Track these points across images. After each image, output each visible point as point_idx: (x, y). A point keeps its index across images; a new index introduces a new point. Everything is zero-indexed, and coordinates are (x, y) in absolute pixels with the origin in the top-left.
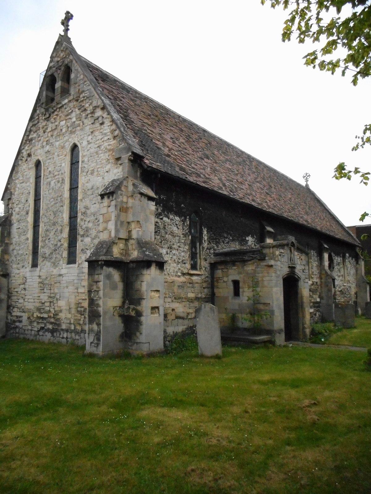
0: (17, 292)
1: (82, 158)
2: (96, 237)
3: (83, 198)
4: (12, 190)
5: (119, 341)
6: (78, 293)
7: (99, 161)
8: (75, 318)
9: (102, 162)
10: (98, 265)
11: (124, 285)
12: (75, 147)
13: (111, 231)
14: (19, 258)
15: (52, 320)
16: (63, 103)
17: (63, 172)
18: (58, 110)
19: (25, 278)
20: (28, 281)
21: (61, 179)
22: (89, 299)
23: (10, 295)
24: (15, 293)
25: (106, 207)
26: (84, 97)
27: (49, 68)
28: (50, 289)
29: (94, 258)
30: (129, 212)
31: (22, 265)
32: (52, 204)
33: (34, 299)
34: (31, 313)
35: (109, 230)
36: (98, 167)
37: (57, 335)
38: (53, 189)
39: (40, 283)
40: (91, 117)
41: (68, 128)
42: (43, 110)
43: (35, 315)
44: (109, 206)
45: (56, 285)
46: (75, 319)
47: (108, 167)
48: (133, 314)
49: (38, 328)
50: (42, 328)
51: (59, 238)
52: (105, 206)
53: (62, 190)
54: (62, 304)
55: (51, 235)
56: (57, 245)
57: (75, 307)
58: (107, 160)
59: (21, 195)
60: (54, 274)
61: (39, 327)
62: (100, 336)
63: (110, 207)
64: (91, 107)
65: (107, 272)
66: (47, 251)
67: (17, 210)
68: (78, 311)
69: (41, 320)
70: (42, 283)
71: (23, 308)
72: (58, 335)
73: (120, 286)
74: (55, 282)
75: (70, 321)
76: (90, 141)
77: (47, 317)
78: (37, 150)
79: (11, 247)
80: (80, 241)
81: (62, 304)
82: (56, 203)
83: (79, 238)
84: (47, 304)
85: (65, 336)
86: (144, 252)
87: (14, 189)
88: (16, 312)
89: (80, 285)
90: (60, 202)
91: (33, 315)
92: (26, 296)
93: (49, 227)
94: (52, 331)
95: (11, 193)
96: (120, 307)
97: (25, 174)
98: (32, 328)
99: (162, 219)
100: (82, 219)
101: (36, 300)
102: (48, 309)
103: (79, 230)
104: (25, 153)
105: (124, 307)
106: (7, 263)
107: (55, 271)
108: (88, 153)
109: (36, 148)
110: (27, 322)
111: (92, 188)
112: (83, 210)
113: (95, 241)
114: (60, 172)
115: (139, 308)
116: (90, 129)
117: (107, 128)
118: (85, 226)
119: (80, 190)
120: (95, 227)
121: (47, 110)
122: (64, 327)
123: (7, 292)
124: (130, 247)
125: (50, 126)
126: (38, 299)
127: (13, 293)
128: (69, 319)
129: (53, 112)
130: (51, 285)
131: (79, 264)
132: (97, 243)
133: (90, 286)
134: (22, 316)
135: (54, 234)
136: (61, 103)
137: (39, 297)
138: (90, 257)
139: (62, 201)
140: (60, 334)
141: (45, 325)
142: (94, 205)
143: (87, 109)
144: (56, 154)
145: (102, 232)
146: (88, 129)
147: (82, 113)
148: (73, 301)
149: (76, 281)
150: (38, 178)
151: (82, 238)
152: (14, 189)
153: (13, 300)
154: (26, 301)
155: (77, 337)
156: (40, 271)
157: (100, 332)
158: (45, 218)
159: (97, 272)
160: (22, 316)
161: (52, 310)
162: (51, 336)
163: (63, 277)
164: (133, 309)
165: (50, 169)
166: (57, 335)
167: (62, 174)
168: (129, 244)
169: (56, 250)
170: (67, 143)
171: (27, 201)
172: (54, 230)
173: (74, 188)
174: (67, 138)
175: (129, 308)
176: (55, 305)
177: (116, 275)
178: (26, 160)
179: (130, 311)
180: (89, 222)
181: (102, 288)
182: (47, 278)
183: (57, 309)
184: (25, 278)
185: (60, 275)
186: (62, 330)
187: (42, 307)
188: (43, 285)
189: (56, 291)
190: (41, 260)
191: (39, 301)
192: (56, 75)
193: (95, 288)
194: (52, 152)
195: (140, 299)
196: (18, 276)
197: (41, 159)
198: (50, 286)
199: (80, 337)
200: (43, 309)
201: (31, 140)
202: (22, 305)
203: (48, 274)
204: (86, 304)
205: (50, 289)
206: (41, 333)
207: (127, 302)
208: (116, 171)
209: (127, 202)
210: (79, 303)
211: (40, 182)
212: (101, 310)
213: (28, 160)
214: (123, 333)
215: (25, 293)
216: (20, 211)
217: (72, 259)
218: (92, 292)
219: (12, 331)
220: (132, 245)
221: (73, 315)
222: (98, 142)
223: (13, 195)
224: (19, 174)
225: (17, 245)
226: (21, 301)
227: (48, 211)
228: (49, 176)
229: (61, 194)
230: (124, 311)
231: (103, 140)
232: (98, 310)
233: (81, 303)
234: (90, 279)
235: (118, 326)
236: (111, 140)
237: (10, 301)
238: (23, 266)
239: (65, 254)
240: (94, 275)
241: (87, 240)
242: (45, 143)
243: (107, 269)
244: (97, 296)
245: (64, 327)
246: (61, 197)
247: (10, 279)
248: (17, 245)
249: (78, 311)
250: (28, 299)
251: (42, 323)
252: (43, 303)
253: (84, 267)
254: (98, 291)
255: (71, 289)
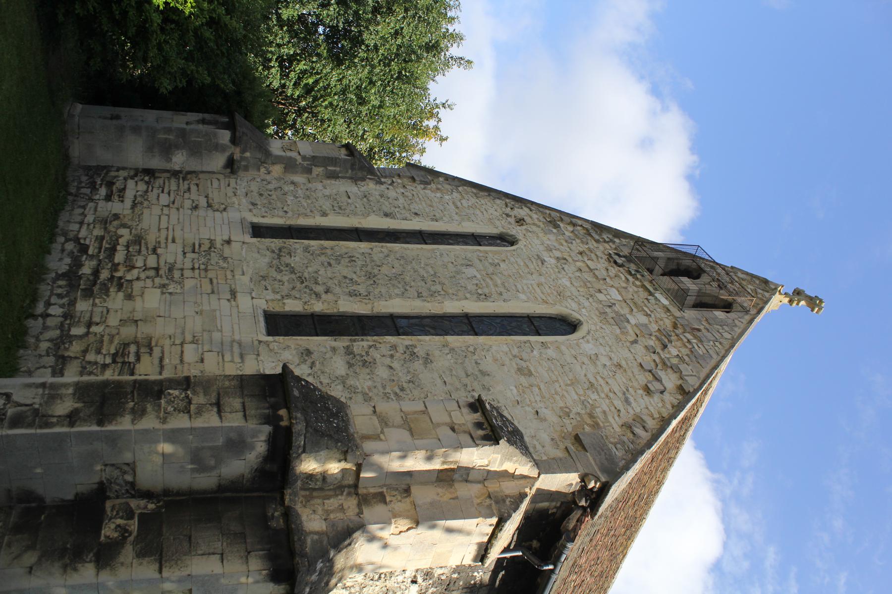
0: (189, 189)
1: (551, 343)
2: (352, 390)
3: (452, 350)
4: (433, 186)
5: (9, 491)
6: (182, 344)
7: (559, 389)
8: (106, 338)
9: (557, 398)
10: (275, 407)
11: (204, 492)
12: (566, 325)
13: (381, 440)
14: (274, 197)
15: (104, 275)
16: (658, 295)
17: (505, 296)
18: (638, 283)
19: (225, 209)
20: (217, 214)
21: (486, 291)
22: (160, 383)
23: (181, 176)
24: (186, 186)
25: (448, 420)
26: (689, 341)
27: (714, 265)
28: (193, 269)
29: (296, 393)
30: (440, 490)
31: (259, 203)
32: (422, 272)
33: (167, 228)
34: (129, 223)
35: (382, 432)
36: (542, 387)
37: (60, 287)
38: (458, 272)
39: (212, 242)
40: (654, 361)
41: (610, 306)
42: (626, 251)
43: (122, 231)
44: (453, 429)
45: (206, 282)
46: (102, 336)
47: (552, 418)
48: (108, 531)
49: (85, 239)
50: (84, 249)
51: (337, 290)
52: (451, 417)
53: (460, 294)
54: (151, 300)
55: (342, 269)
56: (317, 283)
57: (139, 335)
58: (567, 410)
59: (428, 202)
60: (237, 277)
61: (87, 242)
62: (30, 425)
63: (451, 432)
64: (675, 361)
65: (253, 436)
66: (297, 260)
67: (392, 193)
68: (126, 345)
69: (107, 246)
70: (210, 248)
71: (146, 203)
72: (59, 291)
73: (206, 481)
74: (215, 281)
75: (97, 324)
76: (598, 363)
77: (116, 261)
78: (538, 237)
79: (299, 179)
80: (334, 344)
81: (151, 300)
82: (423, 279)
83: (342, 342)
84: (152, 261)
85: (55, 310)
86: (322, 557)
87: (438, 189)
88: (133, 189)
89: (206, 348)
90: (429, 290)
91: (124, 226)
92: (178, 209)
93: (359, 263)
94: (72, 276)
95: (427, 183)
96: (133, 484)
97: (478, 212)
98: (89, 225)
99: (414, 582)
100: (394, 347)
101: (163, 233)
102: (139, 263)
103: (363, 340)
104: (523, 212)
105: (133, 497)
106: (263, 170)
107: (243, 281)
108: (570, 359)
109: (541, 235)
110: (107, 214)
111: (484, 374)
112: (420, 351)
113: (340, 387)
114: (502, 290)
115: (128, 552)
116: (626, 359)
117: (643, 406)
118: (379, 356)
119: (470, 339)
120: (379, 386)
121: (629, 259)
122: (82, 306)
123: (188, 169)
124: (333, 503)
125: (601, 265)
126: (167, 239)
127: (186, 182)
128: (103, 321)
129: (630, 274)
130: (206, 270)
131: (267, 344)
132: (333, 394)
133: (206, 384)
134: (122, 201)
135: (345, 277)
136: (656, 289)
137: (174, 241)
138: (298, 379)
139: (433, 294)
140: (60, 296)
141: (92, 257)
142: (439, 382)
143: (666, 350)
144: (542, 279)
145: (375, 412)
146: (622, 354)
147: (654, 338)
148: (159, 330)
149: (216, 336)
150: (475, 239)
151: (342, 351)
152: (438, 189)
153: (166, 181)
154: (162, 210)
155: (44, 346)
156: (244, 243)
157: (47, 425)
158: (381, 255)
159: (251, 404)
160: (122, 201)
161: (135, 272)
162: (57, 273)
163: (228, 300)
164: (126, 531)
165: (502, 265)
166: (60, 287)
167: (501, 294)
168: (341, 499)
169: (302, 282)
170: (574, 306)
171: (416, 214)
172: (354, 277)
173: (470, 323)
174: (587, 304)
175: (130, 515)
176: (149, 282)
177: (239, 467)
178: (508, 215)
179: (119, 521)
180: (391, 367)
181: (199, 423)
182: (225, 259)
183: (137, 286)
184: (225, 209)
185: (233, 294)
186: (73, 303)
187: (143, 249)
188: (204, 251)
189: (189, 284)
190: (273, 245)
191: (163, 241)
192: (705, 278)
193: (199, 399)
194: (544, 270)
195: (161, 555)
196: (230, 194)
197: (521, 245)
198: (202, 267)
199: (44, 353)
200: (139, 252)
201: (557, 227)
202: (154, 201)
203: (235, 262)
204: (147, 370)
205: (193, 269)
206: (70, 246)
207: (151, 506)
208: (545, 437)
209: (467, 481)
210: (151, 349)
211: (467, 244)
212: (125, 424)
213: (509, 219)
214: (40, 499)
215: (186, 207)
216: (390, 200)
217: (279, 324)
218: (186, 390)
219: (84, 178)
220: (341, 509)
221: (114, 332)
222: (601, 382)
223: (422, 186)
224: (473, 200)
225: (308, 193)
226: (164, 199)
227: (402, 262)
228: (487, 264)
229: (450, 291)
230: (117, 497)
231: (611, 395)
232: (122, 416)
233: (151, 354)
234: (227, 383)
235: (63, 483)
236: (617, 418)
237: (168, 175)
238: (254, 204)
239: (293, 306)
240: (242, 396)
241: (339, 365)
242: (558, 254)
243: (263, 437)
244: (170, 409)
245: (82, 306)
246: (442, 293)
247: (221, 177)
248: (308, 193)
249: (126, 345)
250: (168, 216)
251: (100, 248)
252: (154, 251)
253: (261, 358)
254: (189, 412)
255: (195, 324)
